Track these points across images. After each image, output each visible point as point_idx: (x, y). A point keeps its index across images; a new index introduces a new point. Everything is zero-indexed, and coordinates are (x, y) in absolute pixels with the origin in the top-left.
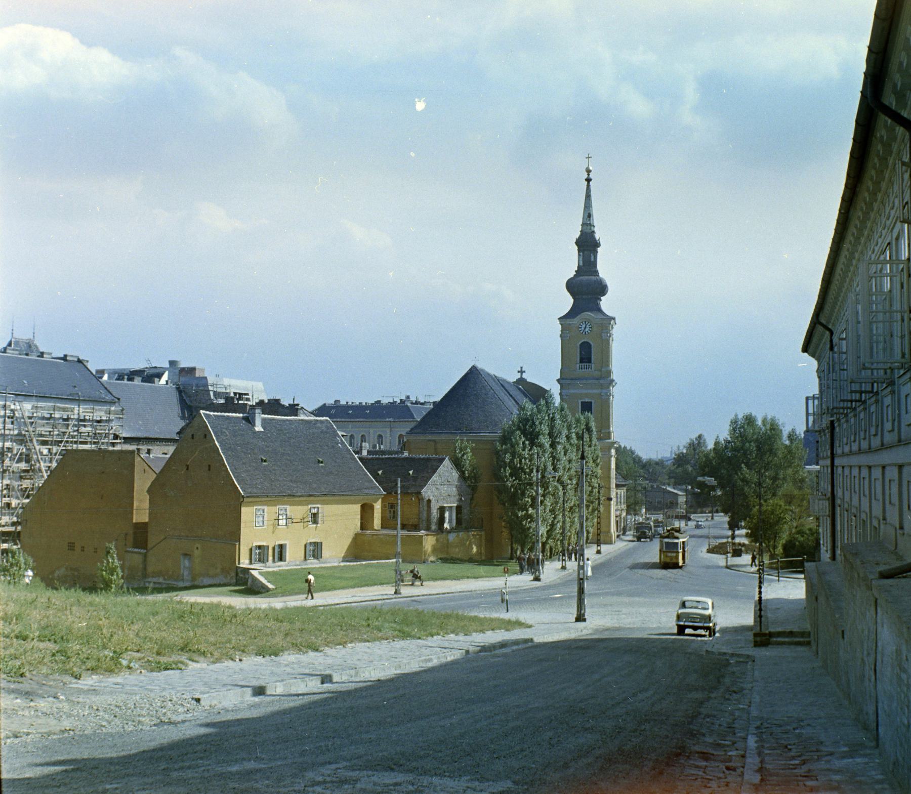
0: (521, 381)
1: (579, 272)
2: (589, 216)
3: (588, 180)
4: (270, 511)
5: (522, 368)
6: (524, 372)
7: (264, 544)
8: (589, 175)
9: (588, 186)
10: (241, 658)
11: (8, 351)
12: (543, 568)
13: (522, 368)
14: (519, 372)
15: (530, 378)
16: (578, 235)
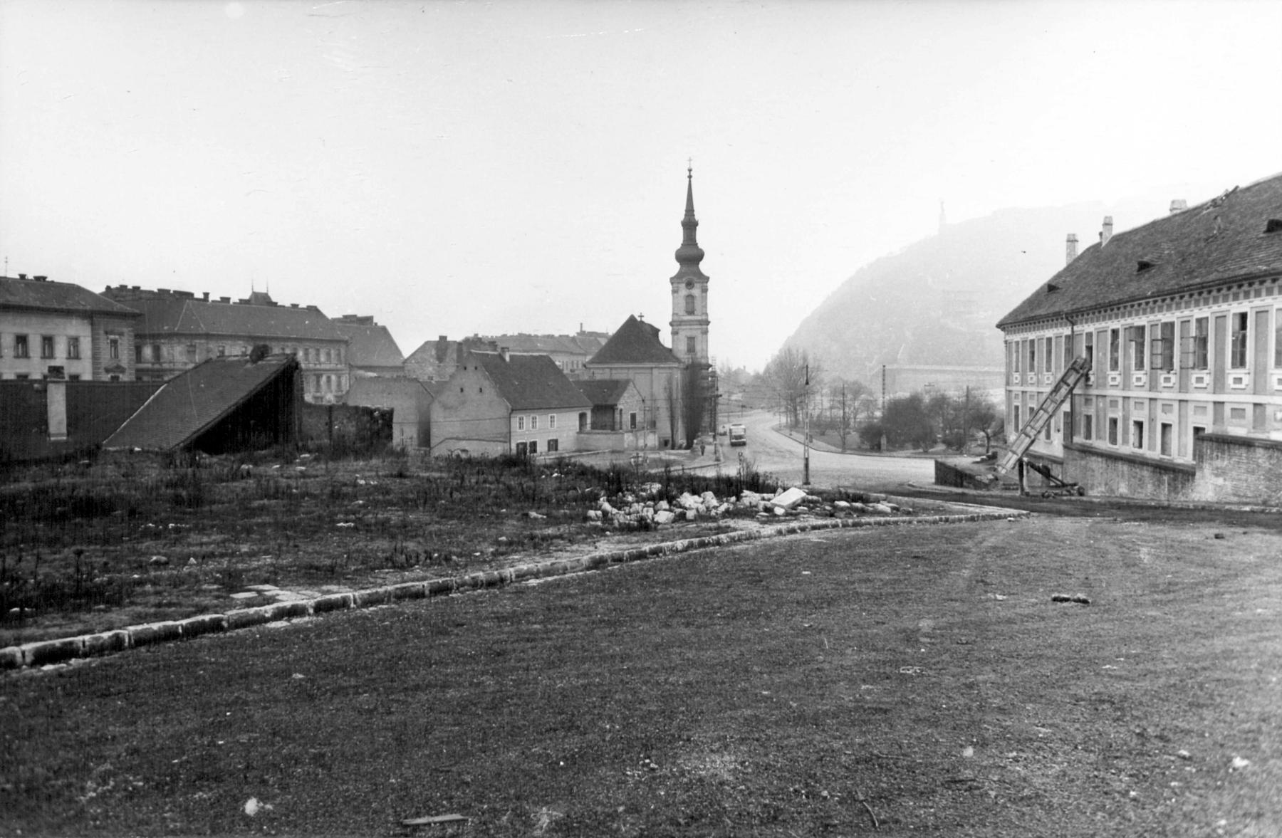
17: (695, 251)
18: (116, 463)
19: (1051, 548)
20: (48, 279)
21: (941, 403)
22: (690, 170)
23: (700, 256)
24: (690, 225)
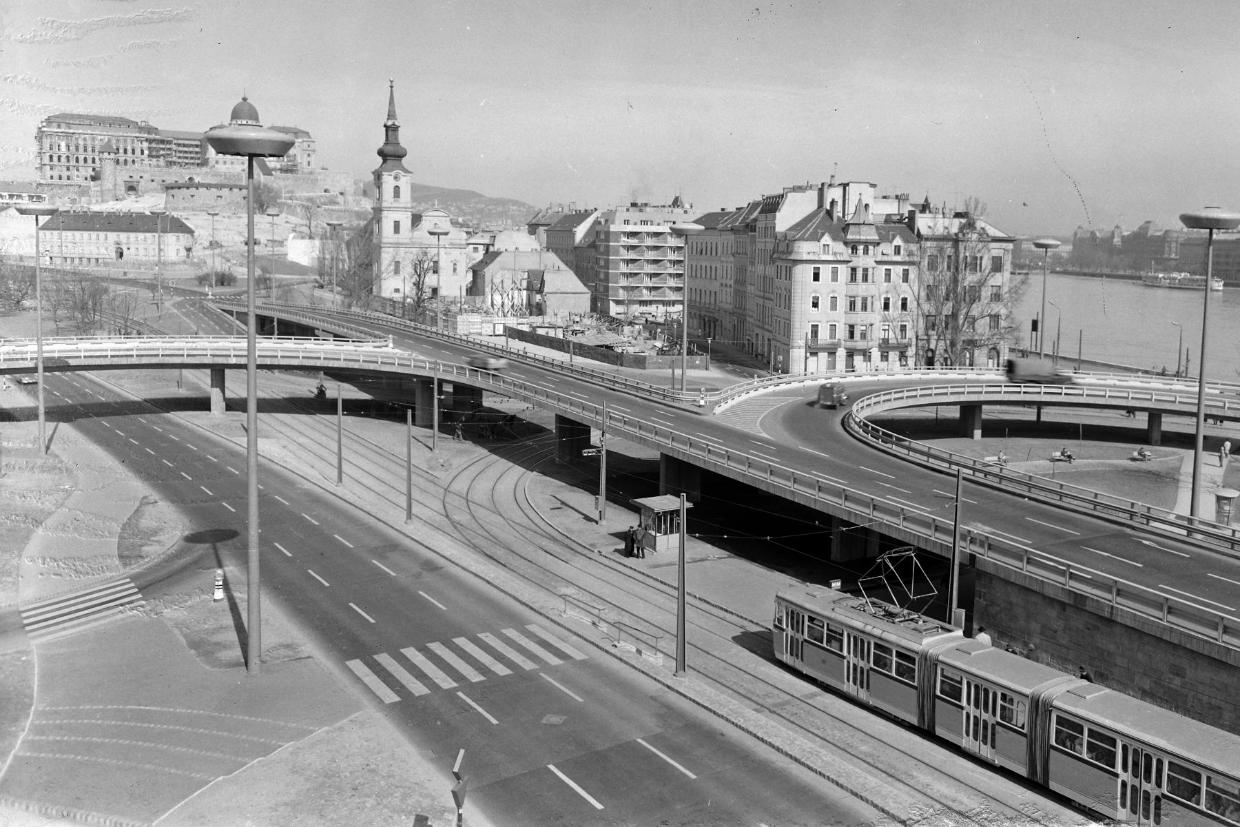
3: (392, 87)
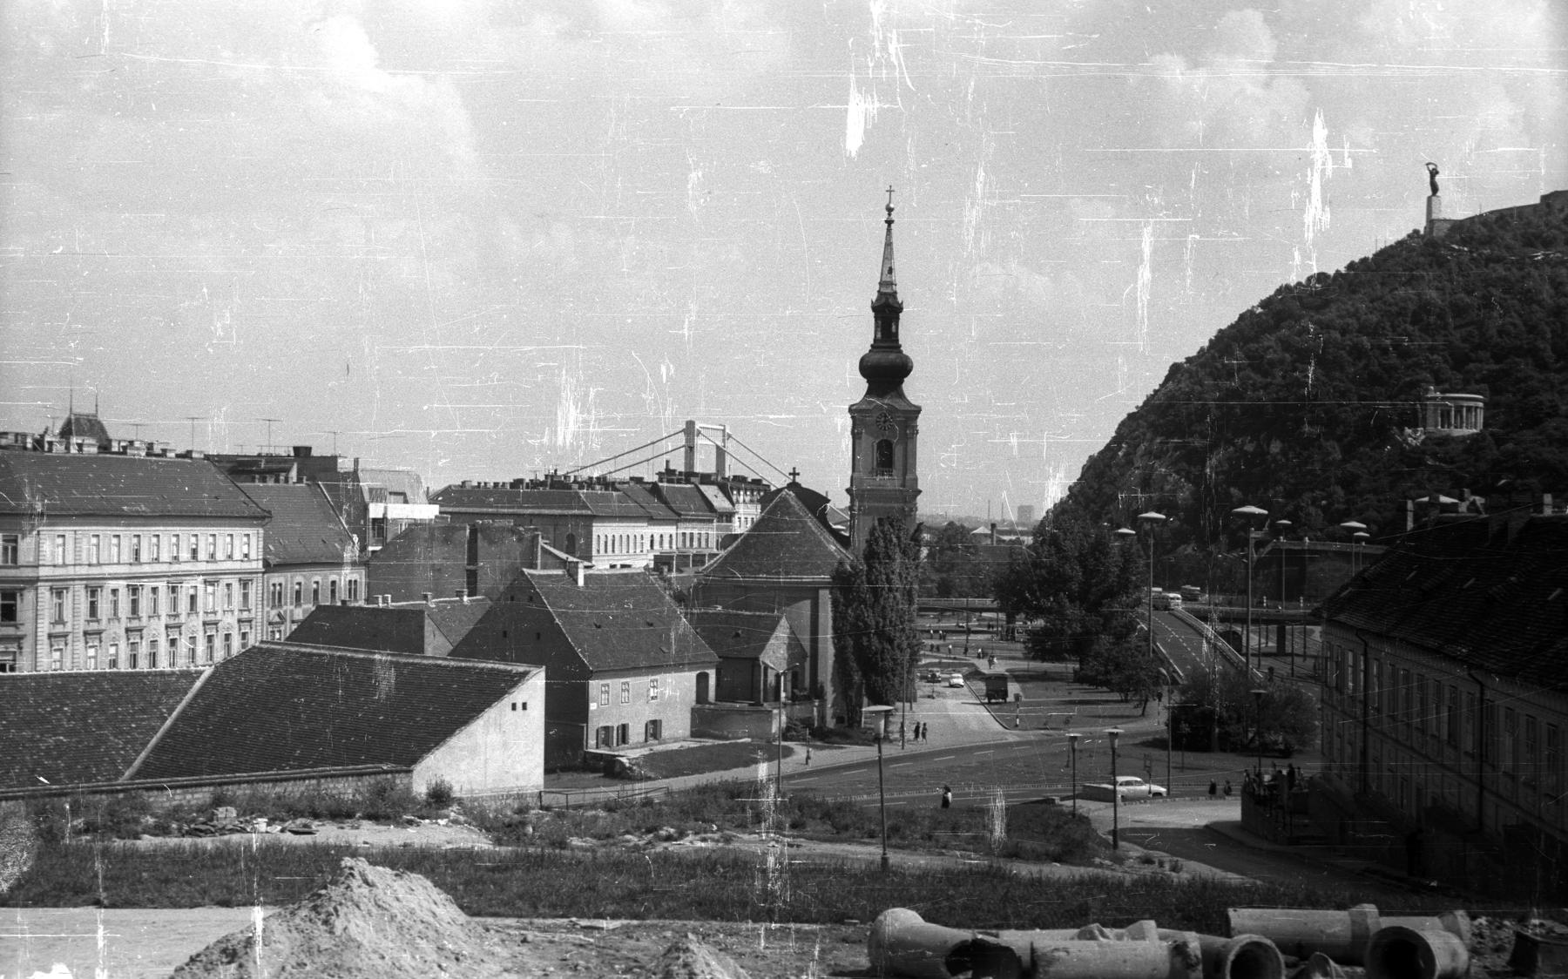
0: (794, 486)
1: (875, 347)
2: (890, 271)
3: (889, 222)
4: (615, 684)
5: (794, 469)
6: (798, 474)
7: (609, 724)
8: (889, 215)
9: (889, 230)
10: (439, 944)
11: (128, 451)
12: (1312, 171)
13: (794, 469)
14: (798, 474)
15: (805, 481)
16: (874, 297)
17: (892, 356)
18: (1284, 727)
19: (990, 186)
20: (314, 453)
21: (846, 129)
22: (890, 210)
23: (904, 368)
24: (887, 311)
